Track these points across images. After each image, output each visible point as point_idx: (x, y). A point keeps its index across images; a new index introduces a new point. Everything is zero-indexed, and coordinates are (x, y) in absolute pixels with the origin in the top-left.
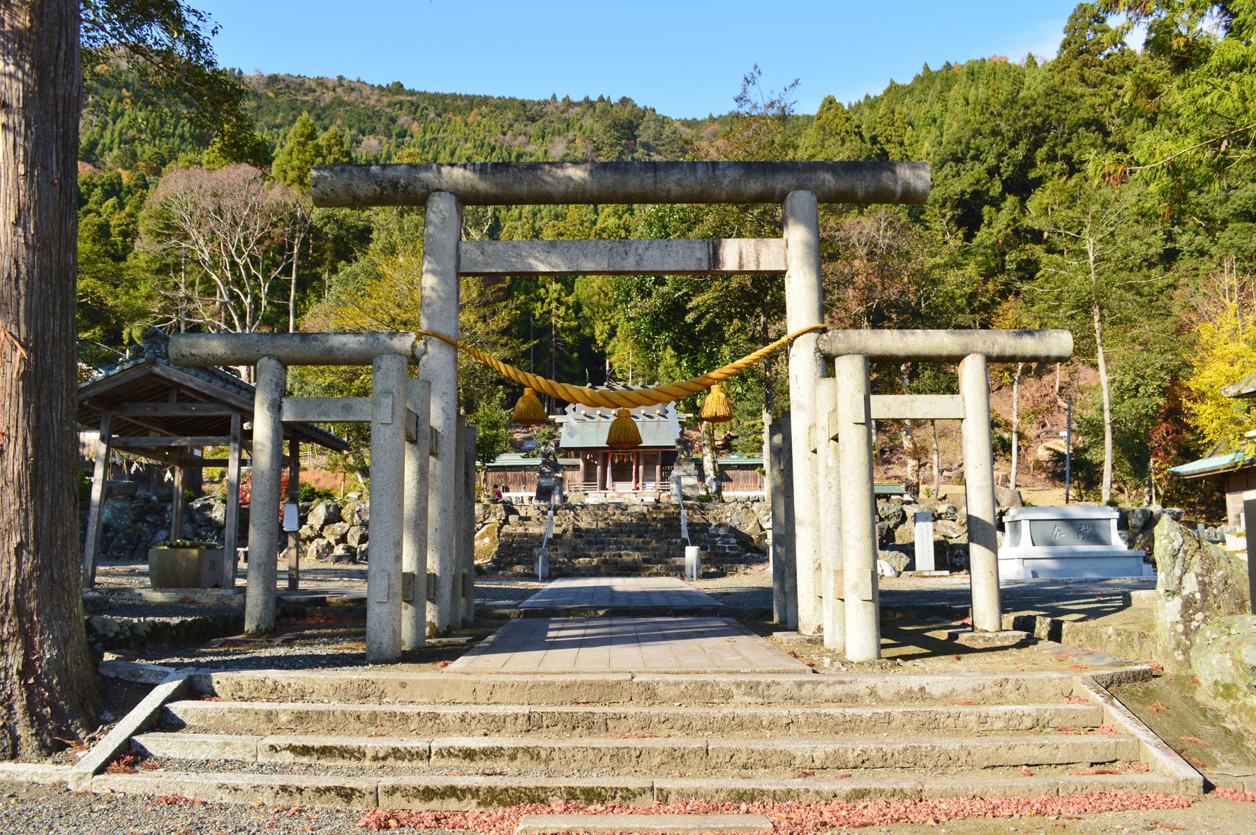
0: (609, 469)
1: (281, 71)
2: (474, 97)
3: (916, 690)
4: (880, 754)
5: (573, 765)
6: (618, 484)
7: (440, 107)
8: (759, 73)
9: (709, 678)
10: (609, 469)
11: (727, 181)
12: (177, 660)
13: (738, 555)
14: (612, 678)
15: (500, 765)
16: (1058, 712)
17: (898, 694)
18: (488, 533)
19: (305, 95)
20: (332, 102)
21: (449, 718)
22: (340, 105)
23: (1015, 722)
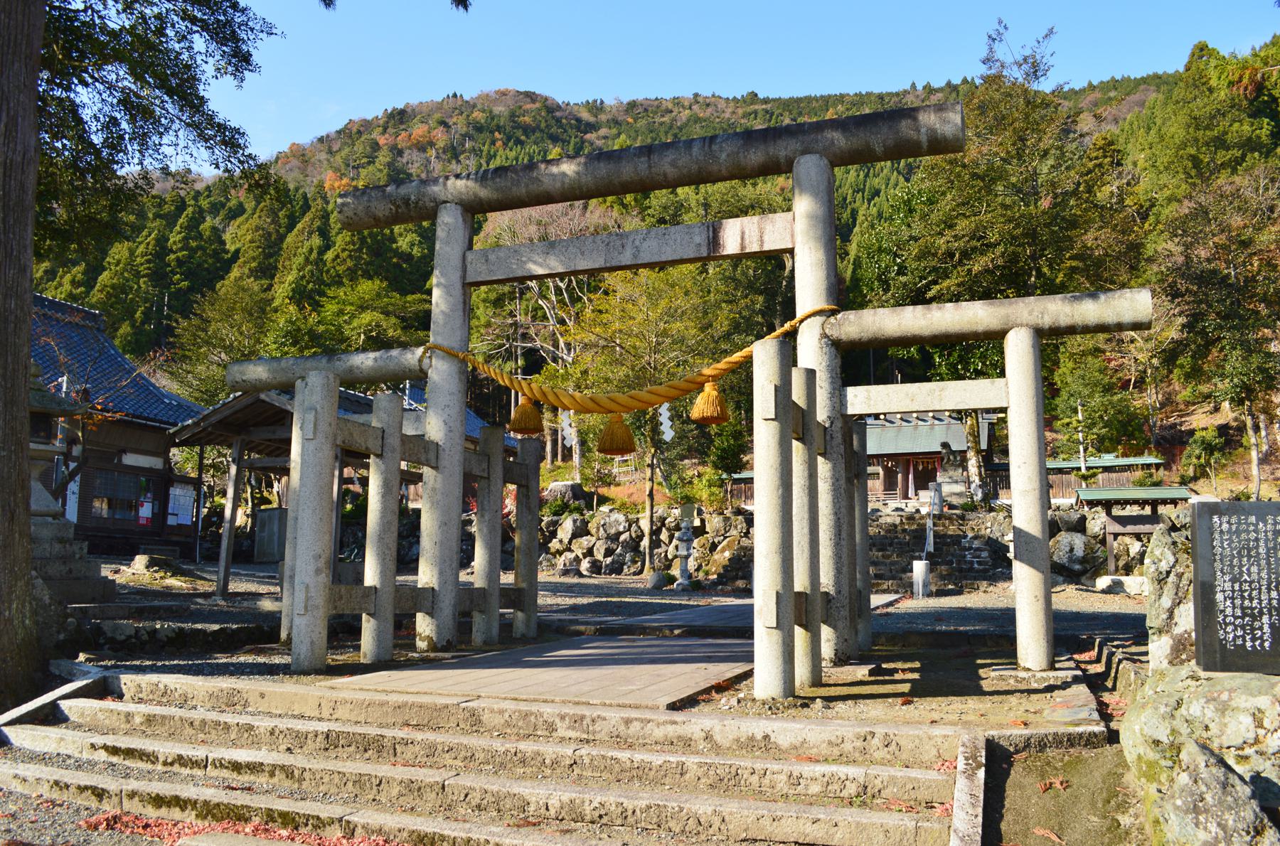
0: (911, 477)
1: (639, 95)
2: (829, 96)
3: (759, 737)
4: (620, 809)
5: (321, 788)
6: (921, 493)
7: (795, 112)
8: (1006, 28)
9: (534, 708)
10: (911, 477)
11: (724, 155)
12: (138, 663)
13: (985, 571)
14: (442, 701)
15: (262, 780)
16: (893, 779)
17: (738, 740)
18: (729, 546)
19: (663, 116)
20: (689, 120)
21: (262, 730)
22: (696, 122)
23: (836, 787)
